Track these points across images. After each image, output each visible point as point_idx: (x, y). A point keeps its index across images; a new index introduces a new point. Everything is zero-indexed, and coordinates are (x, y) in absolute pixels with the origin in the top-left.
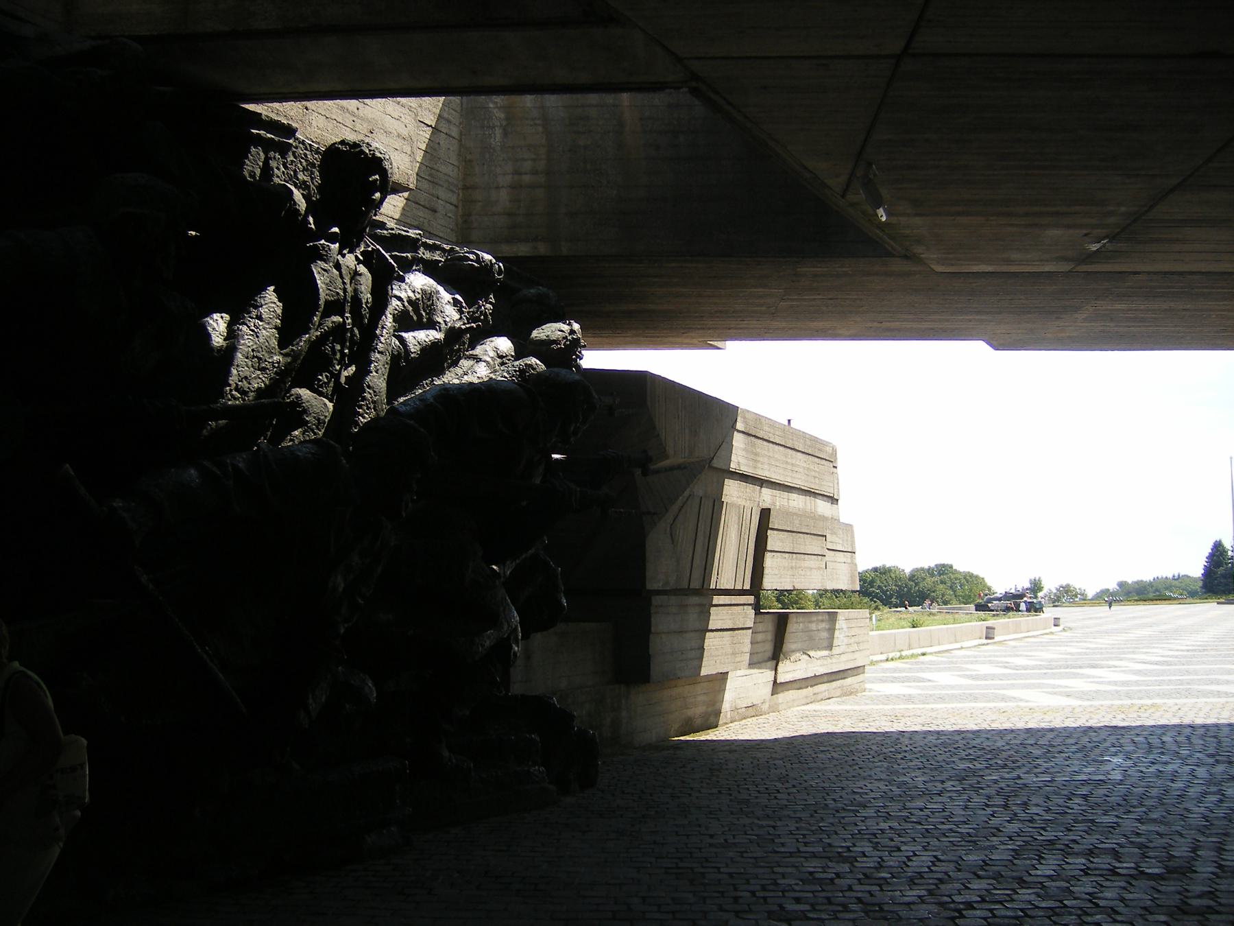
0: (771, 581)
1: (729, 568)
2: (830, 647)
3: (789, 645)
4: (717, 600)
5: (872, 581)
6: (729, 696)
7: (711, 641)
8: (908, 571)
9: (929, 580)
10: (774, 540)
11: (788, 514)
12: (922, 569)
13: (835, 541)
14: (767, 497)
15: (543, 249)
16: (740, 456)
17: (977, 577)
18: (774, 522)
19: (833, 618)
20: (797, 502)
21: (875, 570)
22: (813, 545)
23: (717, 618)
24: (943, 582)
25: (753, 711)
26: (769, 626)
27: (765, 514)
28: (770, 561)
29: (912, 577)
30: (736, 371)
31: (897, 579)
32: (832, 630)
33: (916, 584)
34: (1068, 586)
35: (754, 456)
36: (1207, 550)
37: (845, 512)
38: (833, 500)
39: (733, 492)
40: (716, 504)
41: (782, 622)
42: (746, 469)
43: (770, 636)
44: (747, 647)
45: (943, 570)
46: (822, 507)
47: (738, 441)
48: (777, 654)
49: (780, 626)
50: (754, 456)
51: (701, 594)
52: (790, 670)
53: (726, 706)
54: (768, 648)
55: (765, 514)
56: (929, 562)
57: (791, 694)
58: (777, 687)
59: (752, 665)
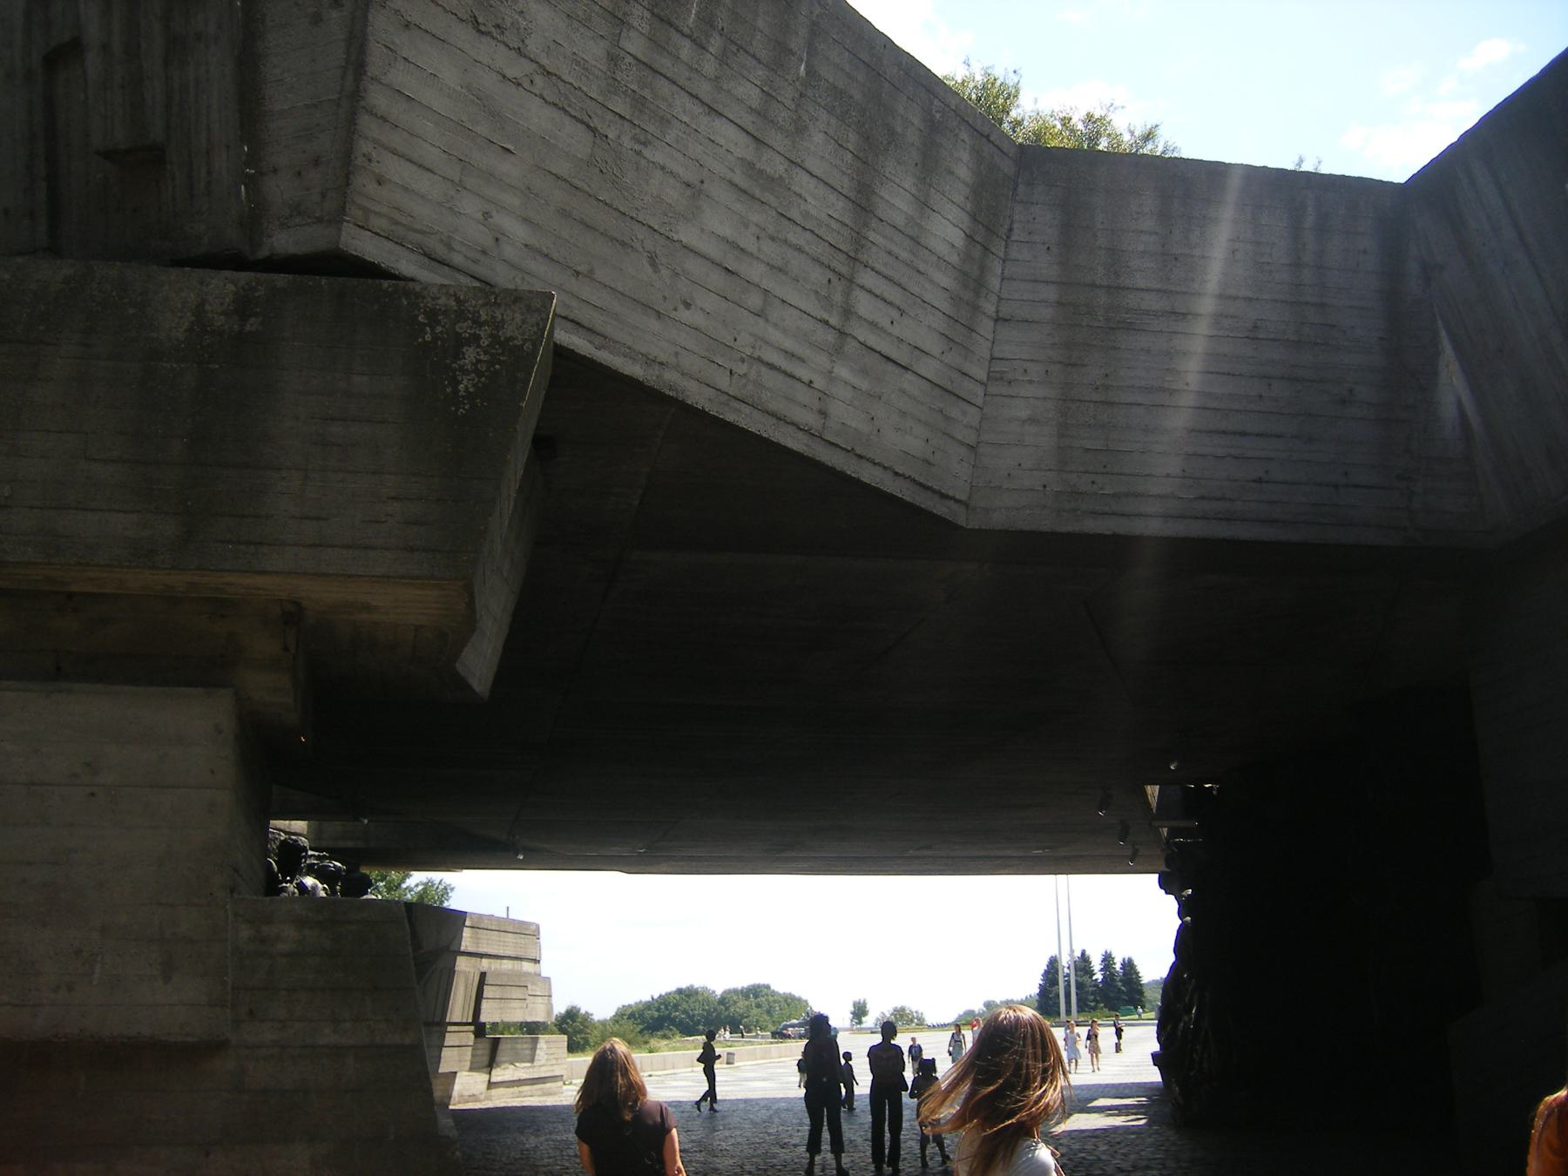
0: (483, 1019)
1: (458, 1009)
2: (532, 1061)
3: (500, 1057)
4: (450, 1028)
5: (676, 1006)
6: (457, 1088)
7: (445, 1053)
8: (719, 992)
9: (742, 1004)
10: (488, 992)
11: (499, 974)
12: (735, 991)
13: (532, 989)
14: (485, 964)
15: (360, 844)
16: (467, 941)
17: (799, 1000)
18: (489, 980)
19: (535, 1041)
20: (507, 965)
21: (680, 991)
22: (517, 993)
23: (450, 1039)
24: (758, 1006)
25: (474, 1098)
26: (484, 1046)
27: (483, 975)
28: (485, 1005)
29: (723, 1000)
30: (474, 890)
31: (707, 1001)
32: (534, 1049)
33: (727, 1009)
34: (903, 1009)
35: (476, 940)
36: (1042, 966)
37: (546, 969)
38: (536, 961)
39: (462, 964)
40: (451, 972)
41: (496, 1043)
42: (470, 949)
43: (487, 1052)
44: (469, 1057)
45: (756, 992)
46: (527, 967)
47: (467, 933)
48: (491, 1064)
49: (491, 1046)
50: (476, 940)
51: (439, 1025)
52: (499, 1075)
53: (455, 1094)
54: (486, 1059)
55: (483, 975)
56: (742, 981)
57: (501, 1090)
58: (491, 1085)
59: (471, 1069)
